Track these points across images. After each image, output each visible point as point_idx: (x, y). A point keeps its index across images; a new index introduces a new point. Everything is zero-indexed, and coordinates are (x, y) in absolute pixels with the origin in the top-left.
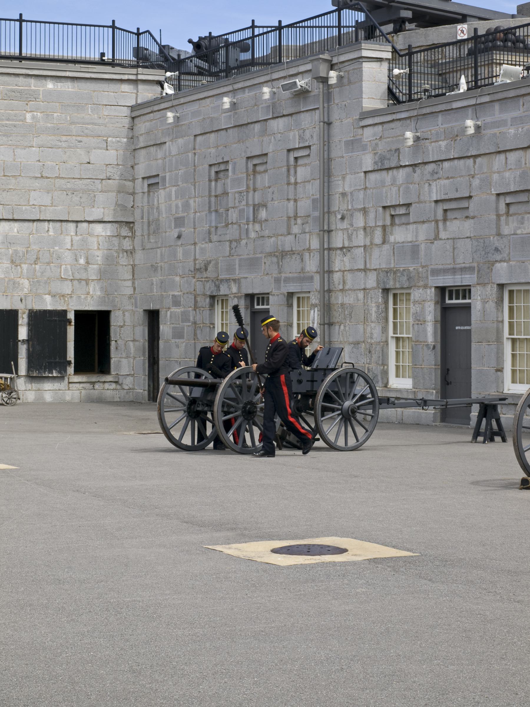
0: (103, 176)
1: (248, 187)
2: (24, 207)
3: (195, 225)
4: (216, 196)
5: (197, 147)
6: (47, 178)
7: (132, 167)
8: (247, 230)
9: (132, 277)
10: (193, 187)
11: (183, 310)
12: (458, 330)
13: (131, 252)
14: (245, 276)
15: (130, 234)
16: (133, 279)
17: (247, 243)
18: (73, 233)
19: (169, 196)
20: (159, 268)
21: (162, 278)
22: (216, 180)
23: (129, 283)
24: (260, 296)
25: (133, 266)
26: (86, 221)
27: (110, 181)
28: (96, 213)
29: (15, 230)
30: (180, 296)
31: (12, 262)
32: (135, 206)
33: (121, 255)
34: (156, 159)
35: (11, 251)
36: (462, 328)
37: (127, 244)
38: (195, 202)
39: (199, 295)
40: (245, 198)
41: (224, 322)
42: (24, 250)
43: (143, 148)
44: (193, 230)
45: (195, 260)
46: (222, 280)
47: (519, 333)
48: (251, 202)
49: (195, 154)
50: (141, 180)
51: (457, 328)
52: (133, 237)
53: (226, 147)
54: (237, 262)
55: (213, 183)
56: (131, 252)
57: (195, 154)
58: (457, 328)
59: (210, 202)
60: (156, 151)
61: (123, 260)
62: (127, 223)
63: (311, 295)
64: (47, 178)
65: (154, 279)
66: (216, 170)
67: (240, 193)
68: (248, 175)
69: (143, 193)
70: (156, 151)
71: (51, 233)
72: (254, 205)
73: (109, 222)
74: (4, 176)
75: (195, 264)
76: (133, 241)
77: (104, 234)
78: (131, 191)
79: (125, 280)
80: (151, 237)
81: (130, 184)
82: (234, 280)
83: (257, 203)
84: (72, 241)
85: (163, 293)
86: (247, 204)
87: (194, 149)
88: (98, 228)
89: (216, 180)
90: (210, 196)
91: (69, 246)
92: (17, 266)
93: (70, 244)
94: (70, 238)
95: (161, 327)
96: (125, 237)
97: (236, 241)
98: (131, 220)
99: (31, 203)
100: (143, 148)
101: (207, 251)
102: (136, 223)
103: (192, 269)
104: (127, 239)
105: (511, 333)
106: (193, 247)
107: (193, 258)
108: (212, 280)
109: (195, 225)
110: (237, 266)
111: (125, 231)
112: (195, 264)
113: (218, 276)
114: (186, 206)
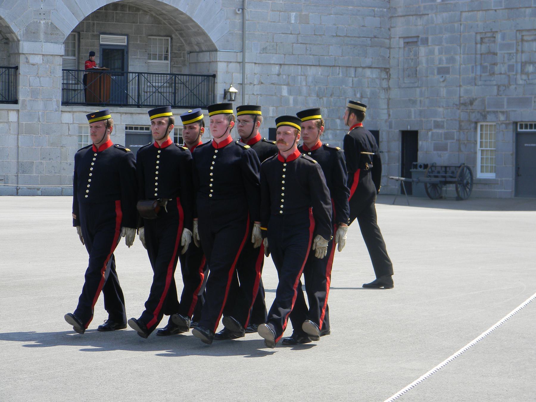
0: (372, 36)
1: (517, 50)
2: (326, 57)
3: (460, 73)
4: (481, 54)
5: (462, 20)
6: (340, 36)
7: (389, 29)
8: (516, 79)
9: (387, 107)
10: (459, 47)
11: (446, 131)
12: (527, 146)
13: (388, 89)
14: (514, 109)
15: (386, 77)
16: (388, 108)
17: (516, 88)
18: (353, 76)
19: (432, 52)
20: (418, 102)
21: (421, 108)
22: (481, 44)
23: (386, 111)
24: (524, 123)
25: (389, 99)
26: (361, 67)
27: (376, 39)
28: (368, 61)
29: (320, 73)
30: (443, 122)
31: (318, 96)
32: (391, 57)
33: (381, 92)
34: (416, 25)
35: (317, 88)
36: (529, 145)
37: (385, 84)
38: (460, 57)
39: (463, 121)
40: (514, 57)
41: (484, 140)
42: (325, 87)
43: (401, 16)
44: (458, 77)
45: (460, 97)
46: (488, 112)
47: (486, 147)
48: (519, 60)
49: (461, 24)
50: (398, 38)
51: (525, 145)
52: (389, 79)
53: (494, 22)
54: (505, 100)
55: (479, 46)
56: (388, 89)
57: (461, 24)
58: (525, 145)
59: (476, 58)
60: (416, 19)
61: (383, 95)
62: (385, 69)
63: (237, 114)
64: (340, 36)
65: (413, 110)
66: (482, 36)
67: (510, 54)
68: (517, 42)
69: (399, 48)
70: (416, 19)
71: (341, 75)
72: (522, 63)
73: (375, 68)
74: (315, 35)
75: (460, 100)
76: (388, 81)
77: (371, 76)
78: (388, 46)
79: (383, 109)
80: (405, 79)
81: (387, 41)
82: (503, 113)
83: (523, 60)
84: (353, 81)
85: (423, 119)
86: (516, 61)
87: (460, 21)
88: (368, 72)
89: (481, 44)
90: (476, 54)
91: (351, 85)
92: (320, 98)
93: (351, 83)
94: (351, 79)
95: (420, 143)
96: (383, 79)
97: (504, 86)
98: (388, 66)
99: (330, 54)
100: (401, 16)
101: (475, 91)
102: (391, 69)
103: (458, 103)
104: (385, 80)
105: (481, 146)
106: (458, 88)
107: (458, 96)
108: (478, 112)
109: (460, 73)
110: (505, 103)
111: (384, 75)
112: (460, 100)
113: (485, 109)
114: (452, 60)
